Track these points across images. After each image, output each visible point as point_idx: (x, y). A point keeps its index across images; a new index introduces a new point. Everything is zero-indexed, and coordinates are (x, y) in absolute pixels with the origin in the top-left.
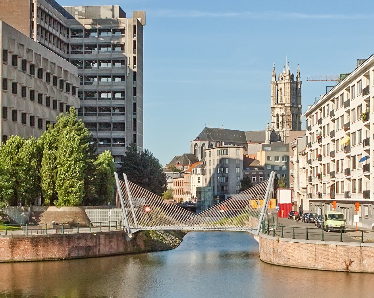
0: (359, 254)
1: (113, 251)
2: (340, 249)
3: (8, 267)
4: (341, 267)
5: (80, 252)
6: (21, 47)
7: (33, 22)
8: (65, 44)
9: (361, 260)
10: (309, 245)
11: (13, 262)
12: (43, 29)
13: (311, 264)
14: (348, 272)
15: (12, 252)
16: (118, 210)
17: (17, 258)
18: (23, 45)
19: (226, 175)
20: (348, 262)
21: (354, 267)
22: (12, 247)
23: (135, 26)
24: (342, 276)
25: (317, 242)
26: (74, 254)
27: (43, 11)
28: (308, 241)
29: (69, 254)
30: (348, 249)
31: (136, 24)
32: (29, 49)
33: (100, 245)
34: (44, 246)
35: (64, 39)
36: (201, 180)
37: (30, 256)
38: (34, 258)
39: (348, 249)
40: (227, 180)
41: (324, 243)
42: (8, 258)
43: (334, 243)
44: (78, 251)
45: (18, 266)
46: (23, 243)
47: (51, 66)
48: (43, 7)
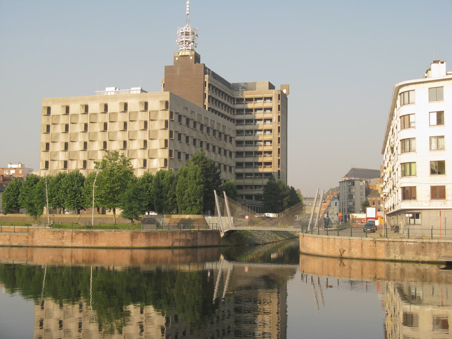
0: (349, 244)
1: (209, 244)
2: (337, 241)
3: (128, 251)
4: (338, 254)
5: (181, 243)
6: (186, 110)
7: (205, 94)
8: (231, 108)
9: (350, 249)
10: (319, 239)
11: (132, 248)
12: (213, 98)
13: (319, 252)
14: (341, 258)
15: (132, 241)
16: (226, 218)
17: (135, 245)
18: (187, 109)
19: (353, 200)
20: (342, 251)
21: (346, 254)
22: (132, 238)
23: (279, 95)
24: (338, 262)
25: (324, 236)
26: (177, 244)
27: (213, 87)
28: (319, 236)
29: (172, 244)
30: (342, 241)
31: (280, 93)
32: (192, 111)
33: (197, 238)
34: (154, 238)
35: (232, 106)
36: (337, 204)
37: (144, 245)
38: (147, 246)
39: (342, 241)
40: (354, 204)
41: (327, 237)
42: (128, 245)
43: (333, 237)
44: (180, 242)
45: (135, 251)
46: (139, 235)
47: (211, 122)
48: (213, 84)
